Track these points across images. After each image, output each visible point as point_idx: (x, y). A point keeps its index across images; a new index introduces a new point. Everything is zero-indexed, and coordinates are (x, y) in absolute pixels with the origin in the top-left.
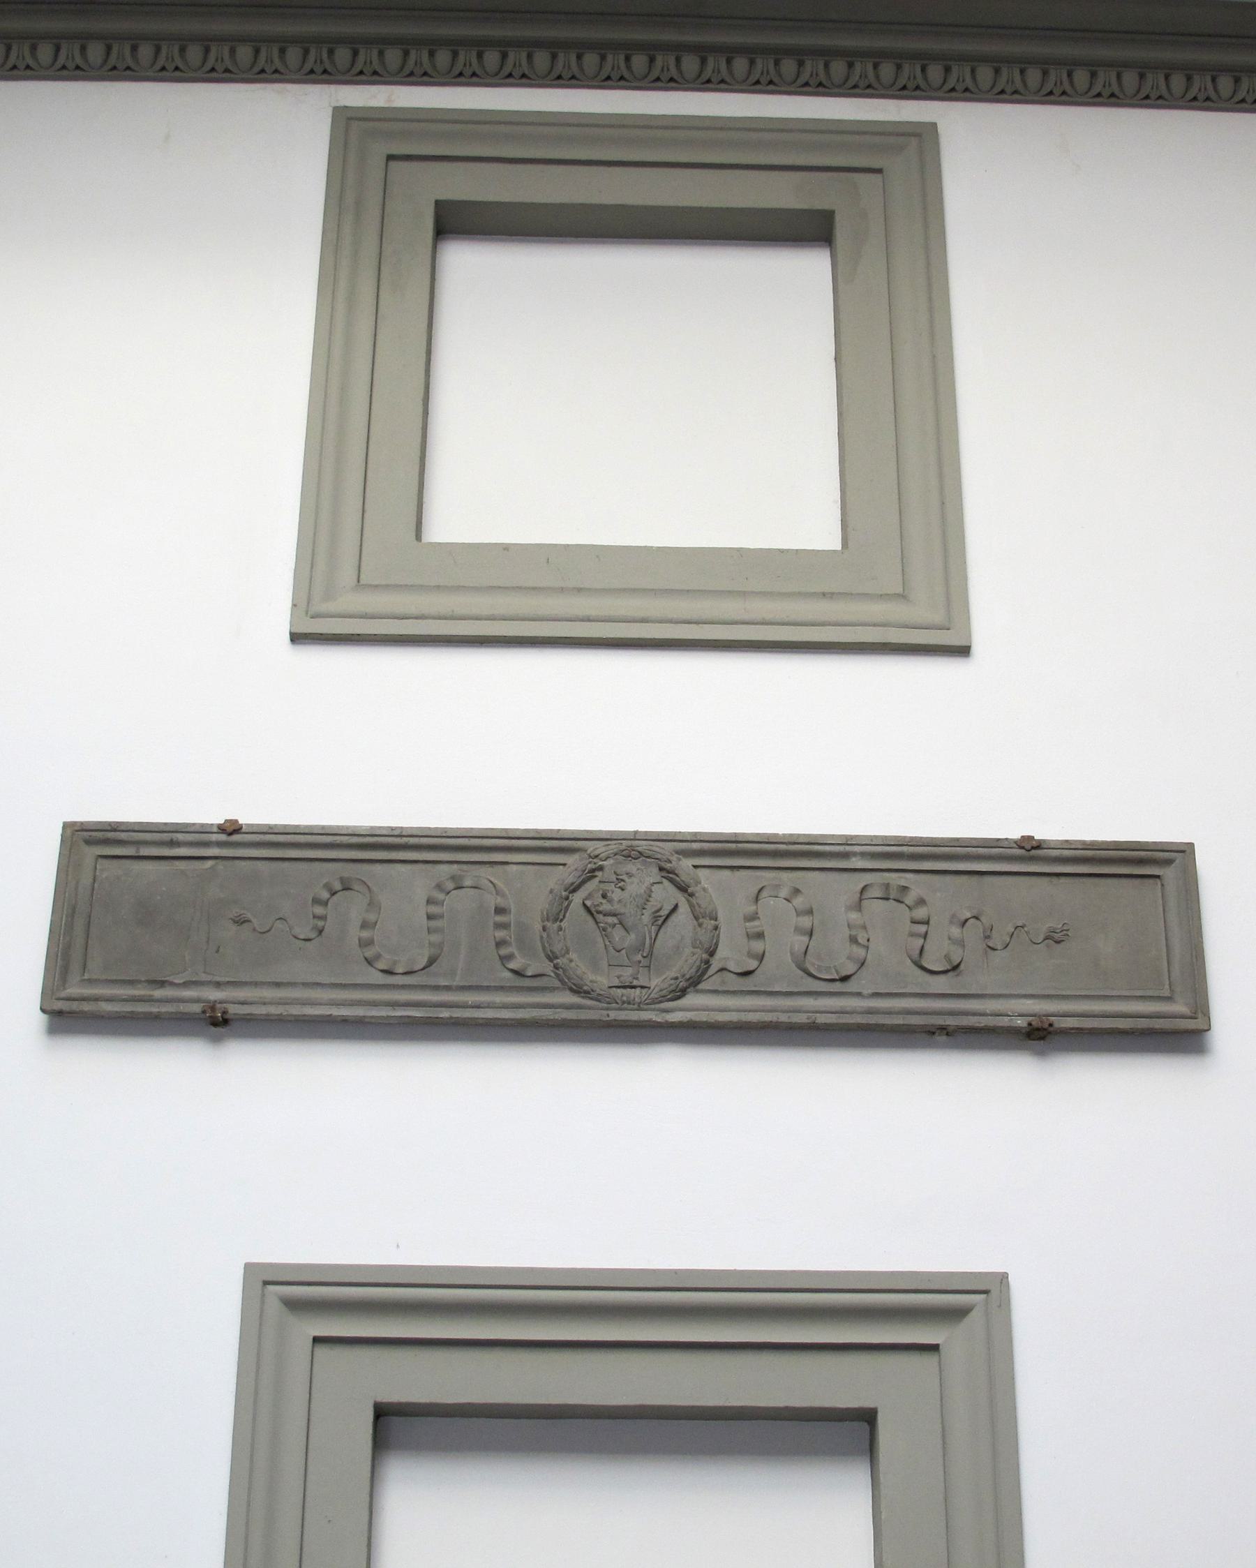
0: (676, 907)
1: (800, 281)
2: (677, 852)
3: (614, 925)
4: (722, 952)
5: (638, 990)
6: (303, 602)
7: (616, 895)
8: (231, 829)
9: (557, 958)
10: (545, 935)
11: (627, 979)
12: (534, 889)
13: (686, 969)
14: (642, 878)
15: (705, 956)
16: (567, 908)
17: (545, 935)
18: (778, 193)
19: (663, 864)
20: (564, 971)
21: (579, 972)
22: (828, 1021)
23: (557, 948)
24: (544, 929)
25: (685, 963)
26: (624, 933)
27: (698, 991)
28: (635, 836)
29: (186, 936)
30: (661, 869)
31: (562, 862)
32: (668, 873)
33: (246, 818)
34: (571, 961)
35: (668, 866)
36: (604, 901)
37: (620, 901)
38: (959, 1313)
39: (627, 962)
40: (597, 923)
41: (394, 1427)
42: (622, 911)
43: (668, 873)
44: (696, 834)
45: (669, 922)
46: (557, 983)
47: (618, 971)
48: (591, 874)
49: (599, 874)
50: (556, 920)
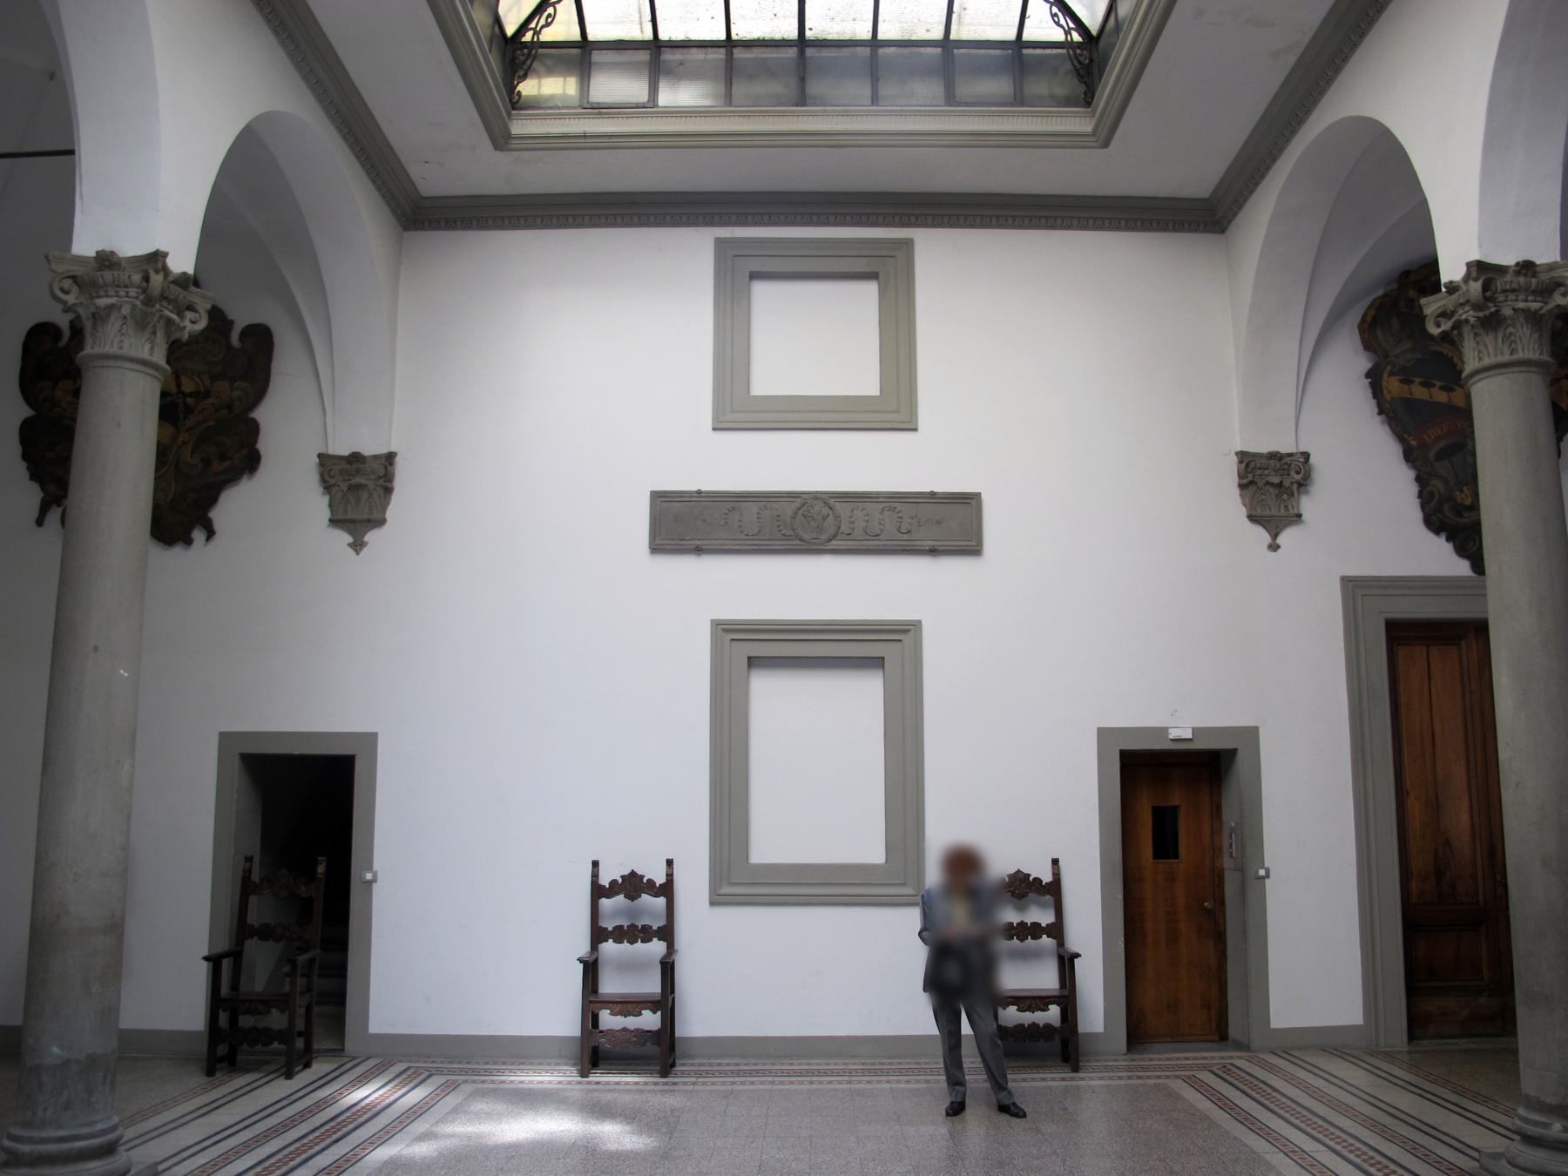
1: (870, 290)
6: (716, 419)
8: (699, 492)
12: (789, 509)
14: (819, 506)
18: (861, 266)
25: (832, 531)
29: (688, 523)
33: (704, 488)
38: (907, 631)
41: (753, 662)
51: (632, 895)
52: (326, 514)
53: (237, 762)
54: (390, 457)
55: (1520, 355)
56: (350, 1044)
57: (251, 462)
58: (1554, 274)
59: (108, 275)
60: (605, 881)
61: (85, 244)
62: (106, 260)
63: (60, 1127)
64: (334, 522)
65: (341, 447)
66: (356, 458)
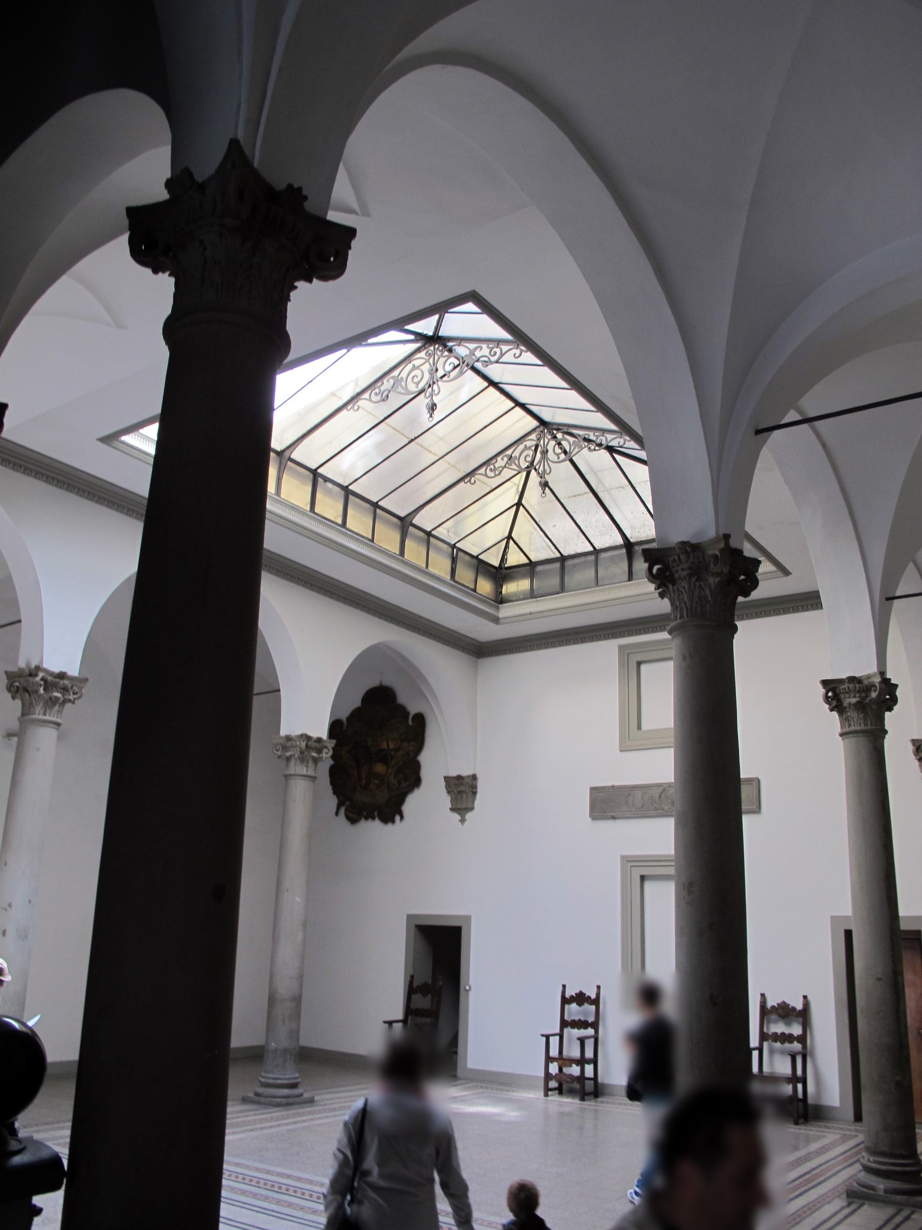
6: (621, 746)
8: (613, 786)
12: (656, 792)
51: (580, 1004)
52: (449, 805)
53: (413, 928)
54: (474, 777)
55: (853, 728)
56: (459, 1073)
57: (416, 782)
58: (870, 680)
59: (289, 744)
60: (567, 996)
61: (283, 733)
62: (288, 738)
63: (274, 1073)
64: (452, 809)
65: (453, 773)
66: (459, 777)
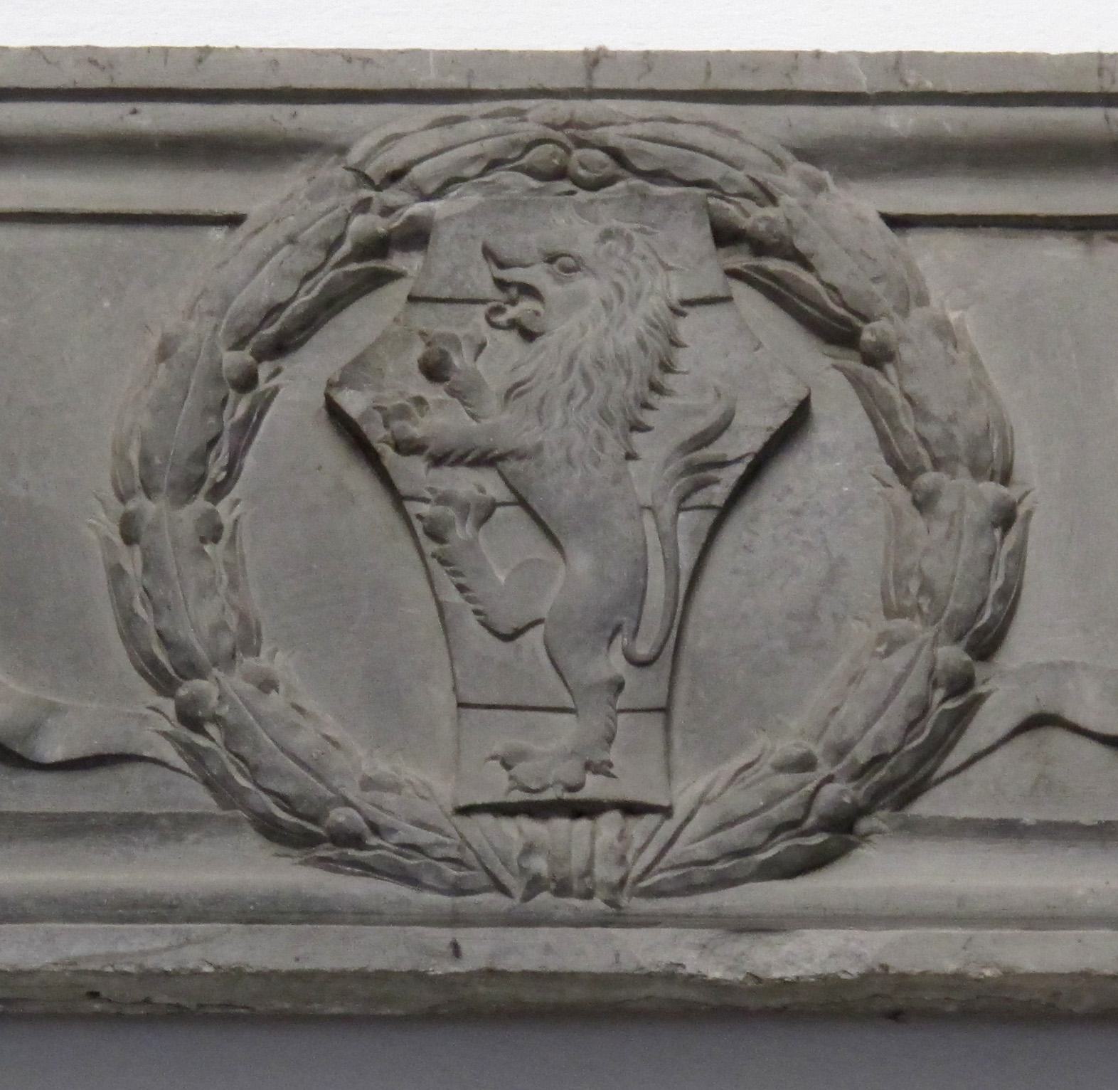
0: (797, 423)
2: (803, 154)
3: (487, 511)
4: (1021, 648)
5: (609, 824)
7: (497, 361)
9: (193, 670)
10: (132, 561)
11: (550, 771)
13: (854, 712)
14: (626, 282)
15: (952, 655)
16: (248, 427)
17: (132, 561)
19: (731, 211)
20: (232, 734)
21: (305, 740)
22: (378, 963)
23: (198, 622)
24: (130, 532)
25: (850, 693)
26: (540, 549)
27: (916, 829)
28: (593, 77)
30: (725, 236)
31: (229, 208)
32: (757, 254)
34: (267, 685)
35: (754, 217)
36: (435, 393)
37: (513, 392)
39: (551, 689)
40: (398, 499)
42: (527, 439)
43: (757, 254)
44: (898, 61)
45: (768, 499)
46: (204, 800)
47: (503, 733)
48: (369, 264)
49: (407, 262)
50: (190, 487)
